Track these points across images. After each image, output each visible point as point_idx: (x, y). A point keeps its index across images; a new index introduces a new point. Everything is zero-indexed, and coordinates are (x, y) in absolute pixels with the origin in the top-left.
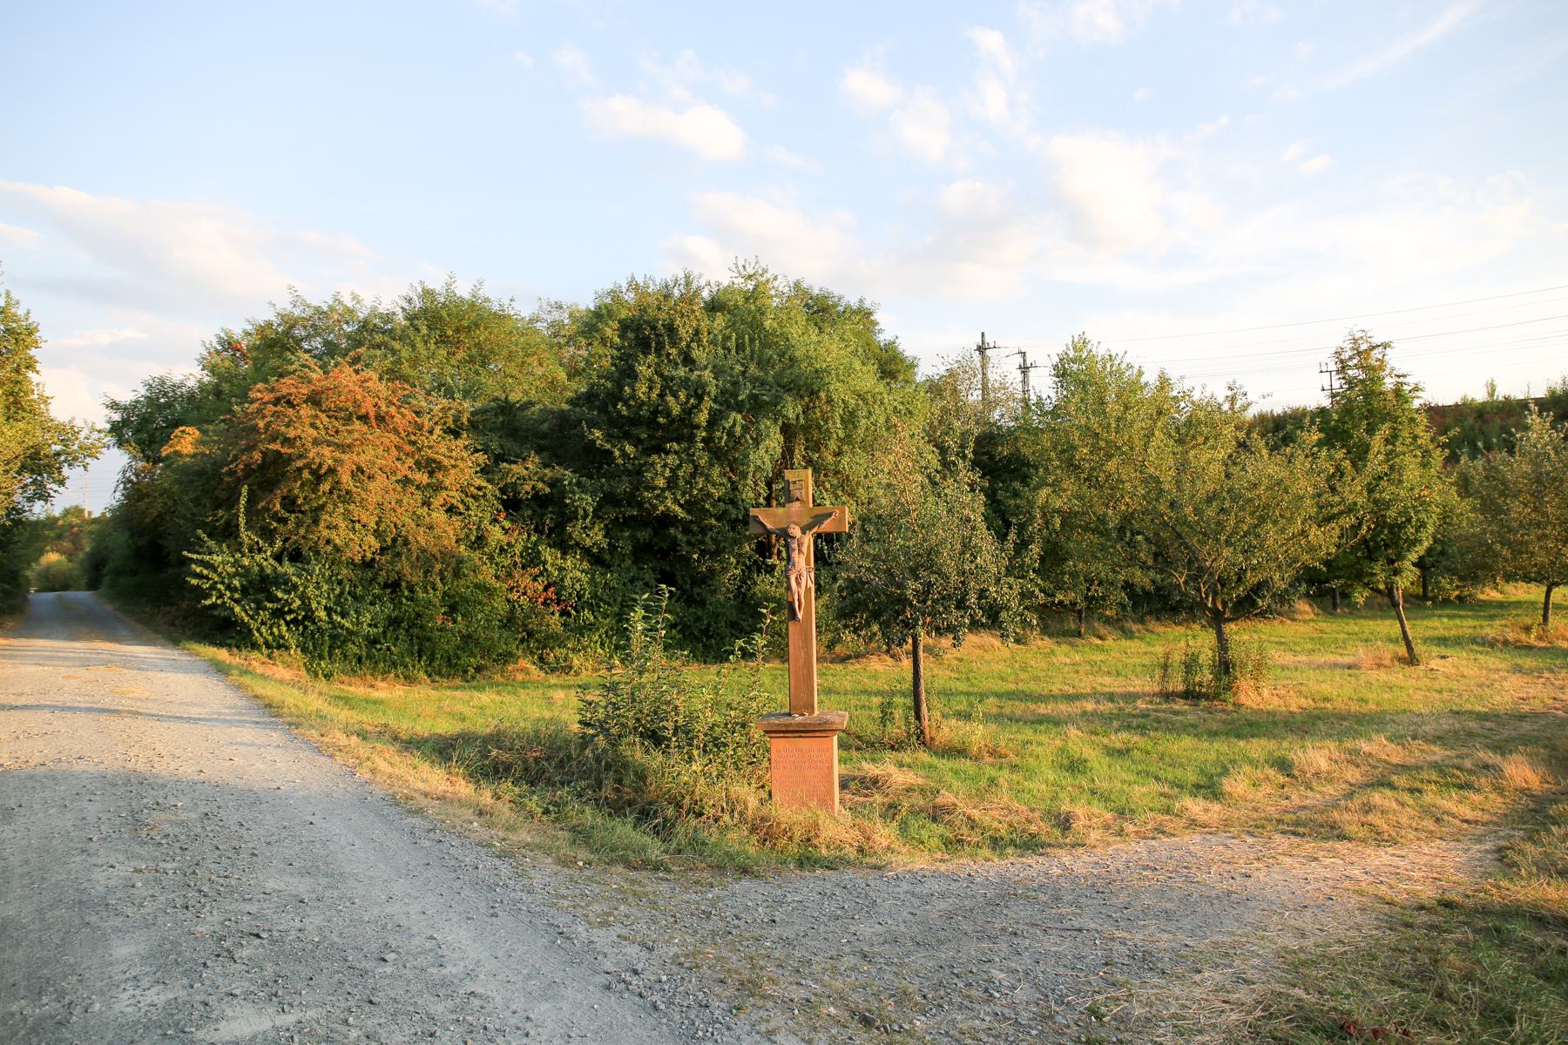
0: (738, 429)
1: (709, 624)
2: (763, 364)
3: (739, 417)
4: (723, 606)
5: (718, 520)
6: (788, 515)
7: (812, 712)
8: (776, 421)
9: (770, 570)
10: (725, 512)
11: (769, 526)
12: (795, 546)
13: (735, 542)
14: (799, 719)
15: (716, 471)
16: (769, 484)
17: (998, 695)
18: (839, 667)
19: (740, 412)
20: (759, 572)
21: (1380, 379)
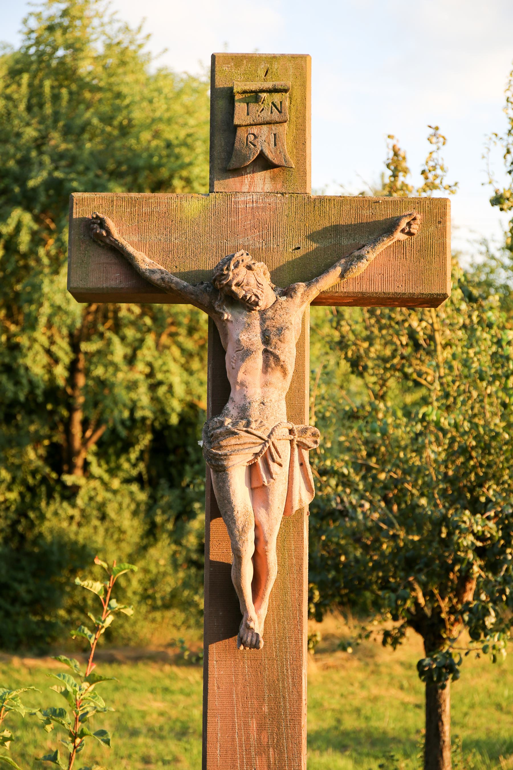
2: (74, 131)
3: (27, 218)
9: (70, 494)
11: (145, 261)
19: (28, 208)
20: (50, 497)
21: (76, 629)
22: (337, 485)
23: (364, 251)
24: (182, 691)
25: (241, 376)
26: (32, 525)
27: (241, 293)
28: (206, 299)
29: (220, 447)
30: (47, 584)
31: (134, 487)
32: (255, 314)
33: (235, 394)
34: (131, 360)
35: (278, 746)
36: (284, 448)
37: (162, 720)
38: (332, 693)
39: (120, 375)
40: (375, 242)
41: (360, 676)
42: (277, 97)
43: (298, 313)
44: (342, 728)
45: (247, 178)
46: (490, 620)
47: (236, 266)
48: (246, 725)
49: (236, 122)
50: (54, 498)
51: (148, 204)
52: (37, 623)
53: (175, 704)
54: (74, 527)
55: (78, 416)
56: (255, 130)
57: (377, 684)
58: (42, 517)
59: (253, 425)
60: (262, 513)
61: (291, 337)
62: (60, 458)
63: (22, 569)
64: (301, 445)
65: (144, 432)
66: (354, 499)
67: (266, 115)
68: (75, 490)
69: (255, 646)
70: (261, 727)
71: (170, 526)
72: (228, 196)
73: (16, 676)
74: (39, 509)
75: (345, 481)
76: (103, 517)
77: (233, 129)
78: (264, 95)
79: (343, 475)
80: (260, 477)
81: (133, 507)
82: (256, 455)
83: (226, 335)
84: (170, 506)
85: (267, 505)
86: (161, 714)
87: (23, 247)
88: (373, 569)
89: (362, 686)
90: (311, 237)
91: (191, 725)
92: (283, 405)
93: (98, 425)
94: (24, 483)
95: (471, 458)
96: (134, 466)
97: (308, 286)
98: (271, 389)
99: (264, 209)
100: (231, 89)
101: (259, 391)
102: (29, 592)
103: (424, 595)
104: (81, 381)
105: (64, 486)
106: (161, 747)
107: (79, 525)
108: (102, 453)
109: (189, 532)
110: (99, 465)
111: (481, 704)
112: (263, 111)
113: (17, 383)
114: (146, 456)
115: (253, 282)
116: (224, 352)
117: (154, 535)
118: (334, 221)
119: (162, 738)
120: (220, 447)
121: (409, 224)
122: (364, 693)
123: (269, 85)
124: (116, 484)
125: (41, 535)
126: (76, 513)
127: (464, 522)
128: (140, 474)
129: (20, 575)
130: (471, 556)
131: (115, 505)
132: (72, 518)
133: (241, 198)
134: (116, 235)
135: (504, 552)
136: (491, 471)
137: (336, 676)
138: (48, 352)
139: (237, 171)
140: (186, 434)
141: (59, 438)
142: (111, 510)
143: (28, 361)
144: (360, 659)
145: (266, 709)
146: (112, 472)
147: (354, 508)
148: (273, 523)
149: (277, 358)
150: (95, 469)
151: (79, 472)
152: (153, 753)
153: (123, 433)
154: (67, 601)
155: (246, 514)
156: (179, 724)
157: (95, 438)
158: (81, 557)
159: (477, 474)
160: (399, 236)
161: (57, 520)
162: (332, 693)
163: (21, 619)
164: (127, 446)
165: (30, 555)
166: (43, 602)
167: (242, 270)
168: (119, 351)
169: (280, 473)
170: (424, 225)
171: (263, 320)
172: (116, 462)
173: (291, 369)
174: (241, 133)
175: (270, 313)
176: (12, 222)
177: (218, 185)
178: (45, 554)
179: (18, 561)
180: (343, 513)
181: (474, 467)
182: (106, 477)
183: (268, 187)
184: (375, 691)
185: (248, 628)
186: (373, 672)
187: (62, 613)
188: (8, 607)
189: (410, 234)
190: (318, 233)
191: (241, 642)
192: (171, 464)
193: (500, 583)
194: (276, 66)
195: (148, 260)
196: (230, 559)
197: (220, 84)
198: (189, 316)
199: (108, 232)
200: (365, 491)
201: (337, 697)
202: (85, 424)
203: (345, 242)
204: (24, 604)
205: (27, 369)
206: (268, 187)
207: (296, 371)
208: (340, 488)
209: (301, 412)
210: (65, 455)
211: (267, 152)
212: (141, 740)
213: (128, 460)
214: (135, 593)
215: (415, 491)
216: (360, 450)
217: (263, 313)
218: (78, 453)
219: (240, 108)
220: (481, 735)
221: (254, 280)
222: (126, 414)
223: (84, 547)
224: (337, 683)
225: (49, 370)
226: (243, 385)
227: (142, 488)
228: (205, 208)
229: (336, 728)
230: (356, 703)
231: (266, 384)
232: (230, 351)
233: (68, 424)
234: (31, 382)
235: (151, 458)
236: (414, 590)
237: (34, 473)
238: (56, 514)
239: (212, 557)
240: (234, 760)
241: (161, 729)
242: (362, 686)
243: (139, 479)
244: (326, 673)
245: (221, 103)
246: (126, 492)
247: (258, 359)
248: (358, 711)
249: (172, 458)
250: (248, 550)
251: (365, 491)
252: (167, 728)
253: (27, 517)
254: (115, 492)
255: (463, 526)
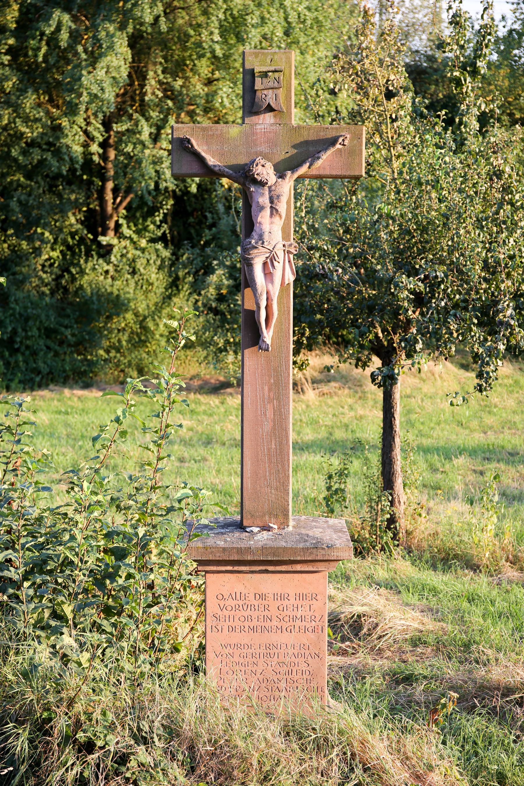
0: (64, 36)
1: (14, 332)
3: (66, 18)
4: (35, 305)
5: (29, 176)
6: (249, 138)
7: (284, 524)
8: (122, 27)
9: (105, 252)
10: (42, 162)
11: (211, 161)
12: (264, 200)
13: (53, 209)
14: (262, 538)
15: (29, 101)
16: (107, 124)
17: (473, 453)
18: (214, 401)
20: (88, 255)
22: (320, 257)
23: (320, 155)
24: (205, 412)
25: (259, 219)
26: (73, 279)
27: (259, 178)
28: (242, 180)
29: (249, 254)
30: (88, 329)
31: (159, 246)
32: (266, 188)
33: (256, 228)
34: (155, 138)
35: (278, 399)
36: (281, 254)
37: (190, 433)
38: (326, 414)
39: (147, 152)
40: (326, 150)
41: (350, 401)
42: (276, 75)
43: (286, 187)
44: (333, 438)
45: (262, 116)
46: (419, 346)
47: (257, 165)
48: (263, 388)
49: (256, 88)
50: (92, 256)
51: (211, 130)
52: (82, 361)
53: (200, 422)
54: (109, 280)
55: (110, 185)
56: (265, 92)
57: (363, 406)
58: (82, 272)
59: (266, 243)
60: (270, 286)
61: (284, 199)
62: (96, 222)
63: (68, 316)
64: (289, 252)
65: (168, 198)
66: (331, 266)
67: (271, 84)
68: (109, 248)
69: (267, 350)
70: (270, 390)
71: (190, 279)
72: (252, 126)
73: (70, 403)
74: (78, 265)
75: (325, 254)
76: (134, 272)
77: (254, 92)
78: (270, 74)
79: (324, 250)
80: (269, 268)
81: (159, 263)
82: (267, 258)
83: (252, 198)
84: (191, 262)
85: (272, 282)
86: (191, 429)
87: (63, 44)
88: (347, 314)
89: (351, 408)
90: (294, 147)
91: (214, 436)
92: (280, 232)
93: (128, 191)
94: (65, 242)
95: (414, 237)
96: (159, 227)
97: (292, 173)
98: (274, 225)
99: (270, 132)
100: (253, 70)
101: (268, 226)
102: (73, 335)
103: (383, 332)
104: (112, 154)
105: (99, 245)
106: (192, 451)
107: (113, 278)
108: (130, 218)
109: (209, 285)
110: (129, 227)
111: (445, 421)
112: (270, 82)
113: (61, 159)
114: (169, 219)
115: (265, 173)
116: (251, 206)
117: (177, 287)
118: (306, 138)
119: (193, 446)
120: (249, 254)
121: (343, 140)
122: (352, 414)
123: (272, 68)
124: (143, 243)
125: (81, 287)
126: (110, 268)
127: (402, 283)
128: (164, 234)
129: (66, 322)
130: (406, 304)
131: (145, 261)
132: (107, 272)
133: (258, 127)
134: (196, 147)
135: (431, 302)
136: (428, 246)
137: (330, 401)
138: (86, 132)
139: (257, 113)
140: (204, 199)
141: (94, 205)
142: (140, 265)
143: (67, 141)
144: (350, 388)
145: (272, 381)
146: (138, 232)
147: (332, 272)
148: (275, 291)
149: (277, 210)
150: (126, 231)
151: (111, 233)
152: (186, 455)
153: (149, 199)
154: (105, 343)
155: (262, 286)
156: (204, 436)
157: (124, 204)
158: (116, 305)
159: (417, 248)
160: (338, 146)
161: (94, 275)
162: (326, 414)
163: (67, 358)
164: (152, 211)
165: (71, 304)
166: (84, 344)
167: (260, 167)
168: (146, 131)
169: (279, 266)
170: (351, 140)
171: (270, 191)
172: (143, 224)
173: (284, 215)
174: (258, 94)
175: (273, 188)
176: (53, 24)
177: (247, 120)
178: (86, 303)
179: (63, 309)
180: (324, 276)
181: (416, 243)
182: (135, 237)
183: (272, 121)
184: (361, 412)
185: (264, 341)
186: (360, 398)
187: (101, 352)
188: (57, 348)
189: (343, 145)
190: (298, 144)
191: (260, 348)
192: (190, 225)
193: (427, 322)
194: (276, 57)
195: (212, 160)
196: (254, 308)
197: (248, 66)
198: (205, 97)
199: (192, 146)
200: (340, 260)
201: (330, 416)
202: (116, 191)
203: (311, 149)
204: (69, 345)
205: (68, 147)
206: (272, 121)
207: (287, 215)
208: (322, 259)
209: (289, 235)
210: (98, 218)
211: (272, 104)
212: (176, 447)
213: (154, 223)
214: (161, 335)
215: (373, 260)
216: (338, 230)
217: (270, 187)
218: (111, 216)
219: (258, 80)
220: (442, 443)
221: (266, 172)
222: (152, 186)
223: (118, 296)
224: (330, 406)
225: (86, 146)
226: (260, 223)
227: (166, 247)
228: (240, 132)
229: (328, 438)
230: (345, 420)
231: (272, 223)
232: (254, 208)
233: (101, 191)
234: (71, 159)
235: (173, 219)
236: (375, 327)
237: (73, 235)
238: (94, 269)
239: (245, 307)
240: (257, 406)
241: (191, 439)
242: (351, 408)
243: (163, 238)
244: (321, 399)
245: (248, 77)
246: (152, 250)
247: (268, 211)
248: (346, 426)
249: (191, 220)
250: (263, 304)
251: (340, 260)
252: (195, 439)
253: (69, 272)
254: (143, 250)
255: (401, 284)
